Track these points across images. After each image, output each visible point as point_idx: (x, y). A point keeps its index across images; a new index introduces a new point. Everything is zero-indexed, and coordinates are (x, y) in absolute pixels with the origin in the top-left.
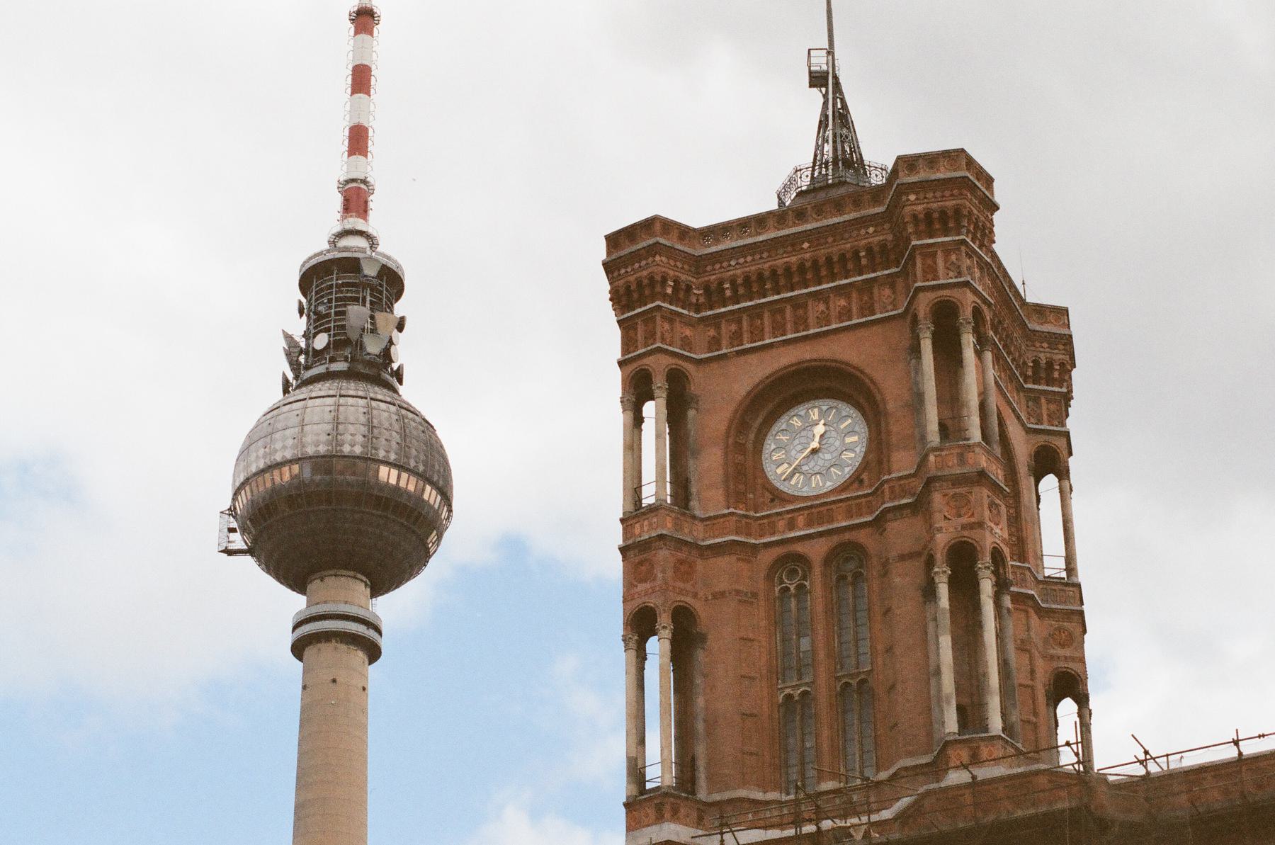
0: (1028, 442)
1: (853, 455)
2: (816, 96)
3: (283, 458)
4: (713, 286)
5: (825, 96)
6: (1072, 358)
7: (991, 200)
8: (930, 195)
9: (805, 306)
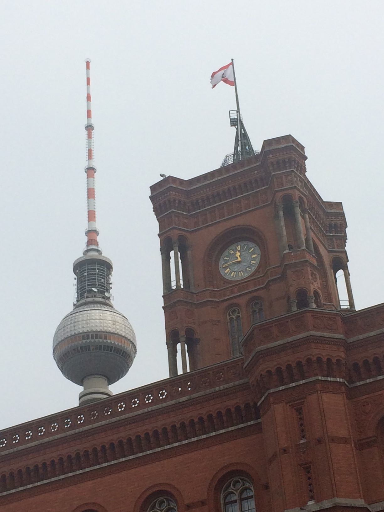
1: (255, 262)
2: (234, 129)
5: (237, 129)
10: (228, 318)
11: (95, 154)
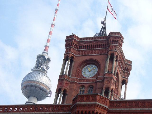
0: (122, 78)
2: (102, 25)
5: (103, 25)
6: (131, 68)
8: (114, 38)
9: (93, 51)
10: (80, 90)
11: (56, 19)
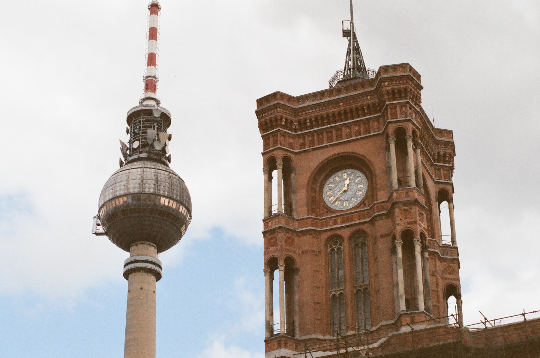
0: (435, 187)
1: (361, 193)
2: (346, 41)
3: (120, 194)
4: (302, 121)
5: (350, 41)
6: (454, 152)
7: (420, 85)
8: (394, 83)
9: (341, 130)
